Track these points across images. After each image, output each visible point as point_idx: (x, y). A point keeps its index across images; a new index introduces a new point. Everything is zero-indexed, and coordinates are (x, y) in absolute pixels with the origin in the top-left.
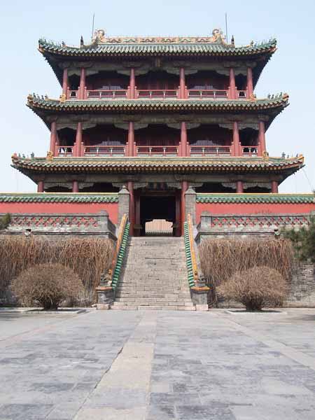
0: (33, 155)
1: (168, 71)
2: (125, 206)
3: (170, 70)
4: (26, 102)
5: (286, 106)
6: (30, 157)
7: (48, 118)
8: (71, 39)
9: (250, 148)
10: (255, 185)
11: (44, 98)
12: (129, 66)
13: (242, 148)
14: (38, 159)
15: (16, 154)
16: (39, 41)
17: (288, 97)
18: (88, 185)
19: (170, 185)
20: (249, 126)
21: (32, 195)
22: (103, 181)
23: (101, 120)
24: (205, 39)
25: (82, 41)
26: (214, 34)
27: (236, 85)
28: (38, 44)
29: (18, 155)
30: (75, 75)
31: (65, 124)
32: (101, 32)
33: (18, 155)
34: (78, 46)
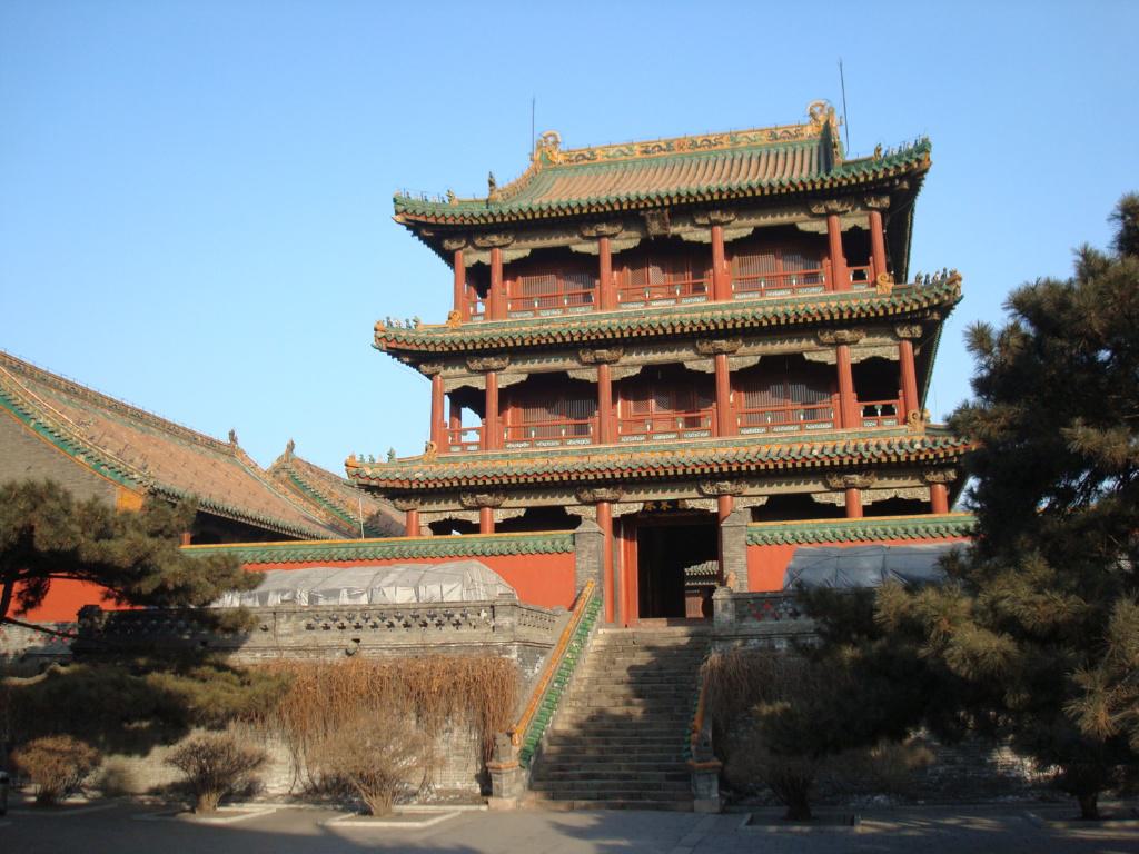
0: (391, 455)
1: (685, 237)
2: (255, 512)
3: (690, 233)
4: (372, 341)
5: (956, 303)
6: (385, 459)
7: (447, 244)
8: (462, 185)
9: (878, 405)
10: (893, 495)
11: (412, 324)
12: (594, 234)
13: (860, 408)
14: (401, 461)
15: (353, 457)
16: (395, 201)
17: (960, 279)
18: (514, 514)
19: (690, 504)
20: (878, 352)
21: (321, 474)
22: (545, 508)
23: (537, 365)
24: (792, 131)
25: (491, 184)
26: (812, 115)
27: (846, 253)
28: (393, 204)
29: (358, 459)
30: (479, 263)
31: (456, 377)
32: (551, 140)
33: (358, 459)
34: (483, 193)
